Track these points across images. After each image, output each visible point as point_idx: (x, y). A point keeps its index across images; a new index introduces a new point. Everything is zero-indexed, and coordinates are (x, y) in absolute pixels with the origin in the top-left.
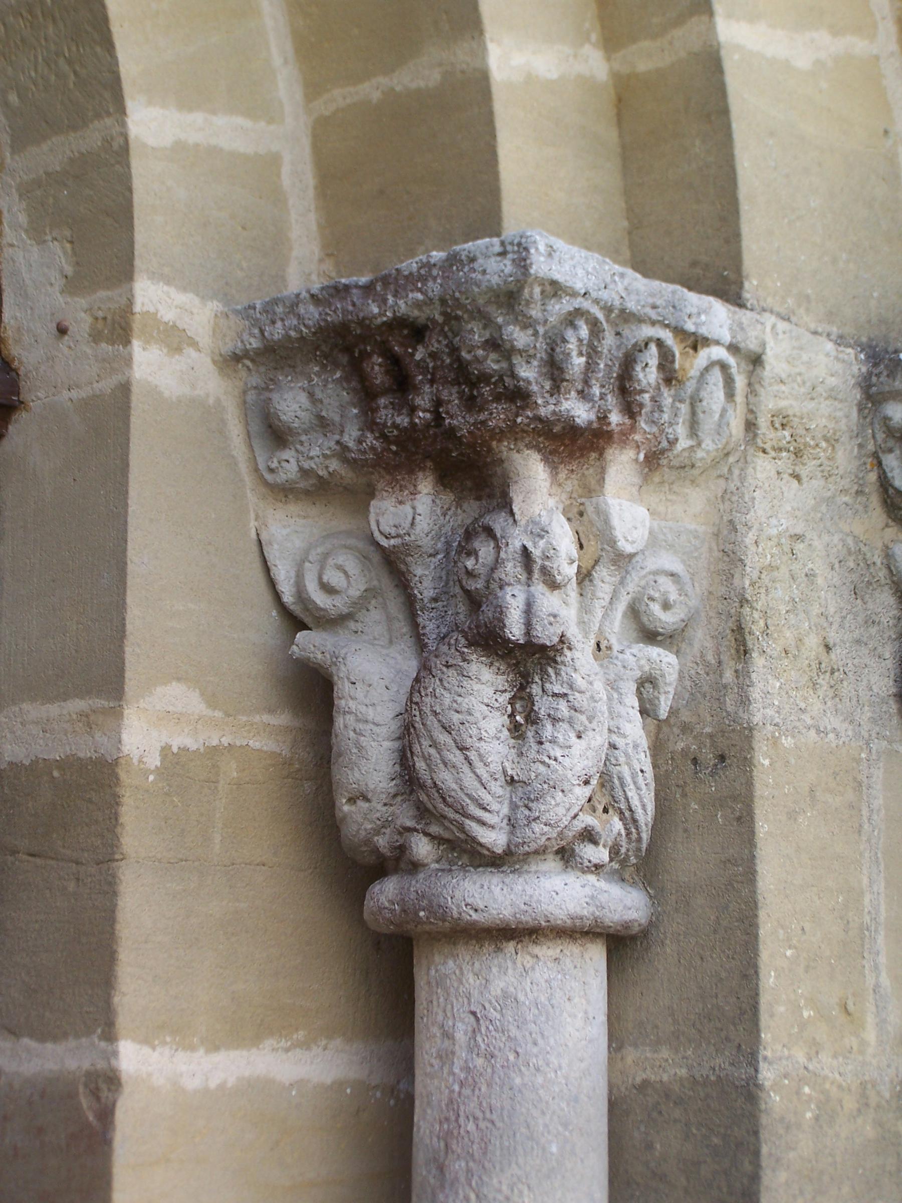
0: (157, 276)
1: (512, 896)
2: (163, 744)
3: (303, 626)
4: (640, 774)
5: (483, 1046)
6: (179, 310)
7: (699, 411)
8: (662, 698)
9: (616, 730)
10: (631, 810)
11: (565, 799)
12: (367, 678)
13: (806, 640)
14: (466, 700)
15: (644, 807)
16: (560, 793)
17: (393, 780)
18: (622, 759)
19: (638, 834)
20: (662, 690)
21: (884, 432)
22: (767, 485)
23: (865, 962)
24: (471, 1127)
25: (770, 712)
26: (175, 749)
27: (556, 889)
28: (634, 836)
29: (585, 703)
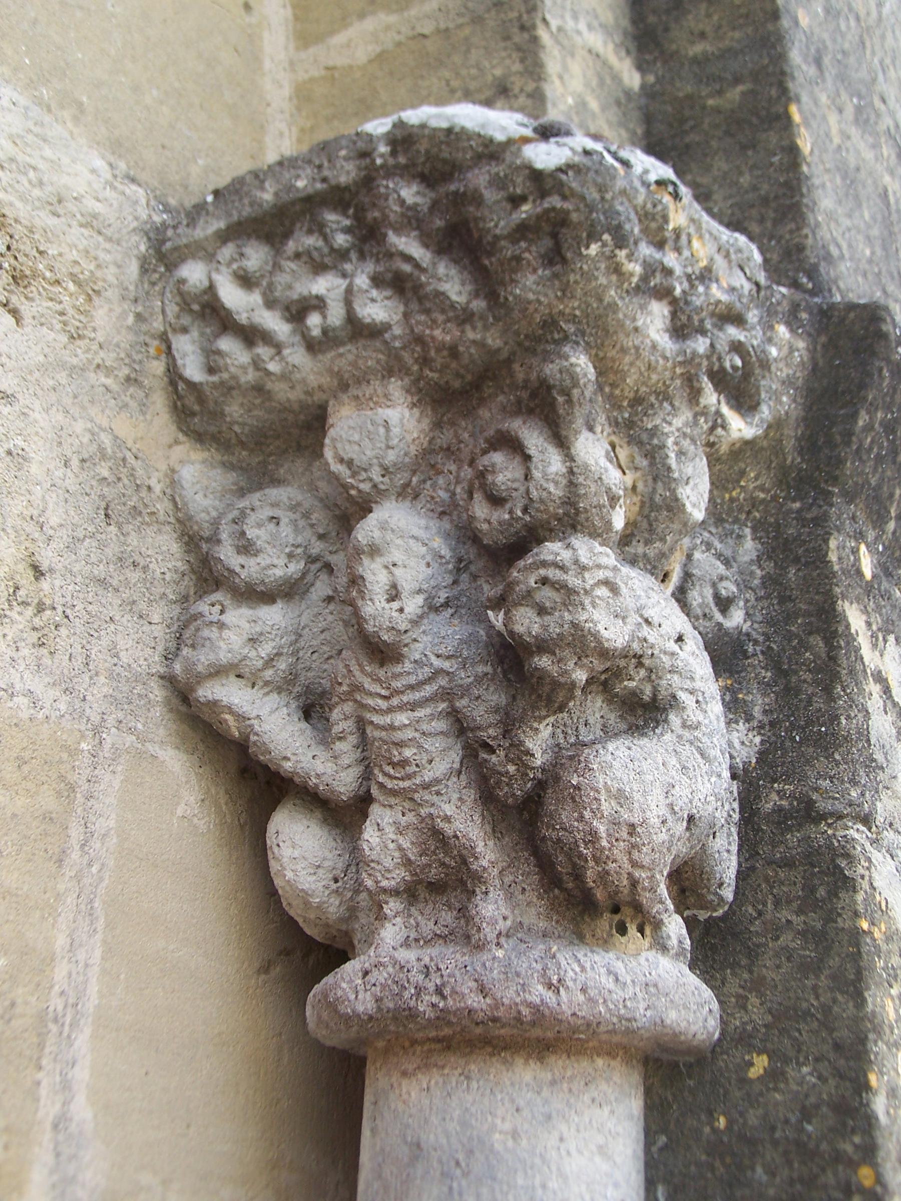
21: (177, 304)
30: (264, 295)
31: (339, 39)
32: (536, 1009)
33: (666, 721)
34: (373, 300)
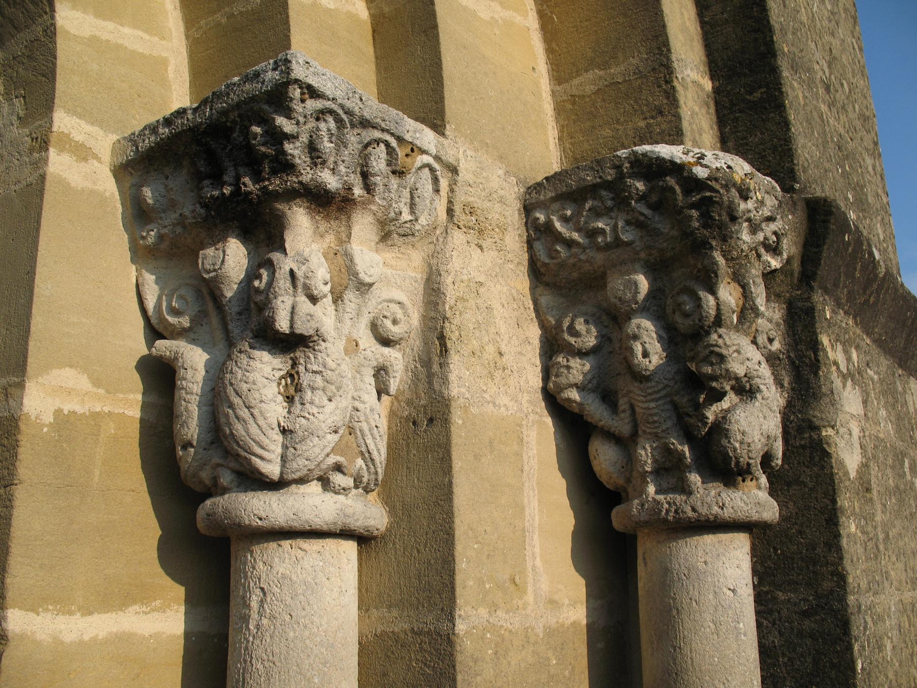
1: (285, 509)
2: (56, 408)
3: (162, 337)
4: (375, 429)
5: (268, 611)
6: (87, 136)
8: (392, 381)
10: (369, 452)
13: (486, 348)
14: (252, 375)
15: (378, 450)
16: (317, 438)
18: (362, 418)
19: (375, 468)
20: (391, 375)
22: (460, 248)
24: (260, 666)
25: (463, 390)
26: (66, 412)
28: (372, 470)
29: (335, 378)
30: (574, 225)
31: (576, 82)
32: (716, 517)
33: (756, 397)
34: (627, 231)
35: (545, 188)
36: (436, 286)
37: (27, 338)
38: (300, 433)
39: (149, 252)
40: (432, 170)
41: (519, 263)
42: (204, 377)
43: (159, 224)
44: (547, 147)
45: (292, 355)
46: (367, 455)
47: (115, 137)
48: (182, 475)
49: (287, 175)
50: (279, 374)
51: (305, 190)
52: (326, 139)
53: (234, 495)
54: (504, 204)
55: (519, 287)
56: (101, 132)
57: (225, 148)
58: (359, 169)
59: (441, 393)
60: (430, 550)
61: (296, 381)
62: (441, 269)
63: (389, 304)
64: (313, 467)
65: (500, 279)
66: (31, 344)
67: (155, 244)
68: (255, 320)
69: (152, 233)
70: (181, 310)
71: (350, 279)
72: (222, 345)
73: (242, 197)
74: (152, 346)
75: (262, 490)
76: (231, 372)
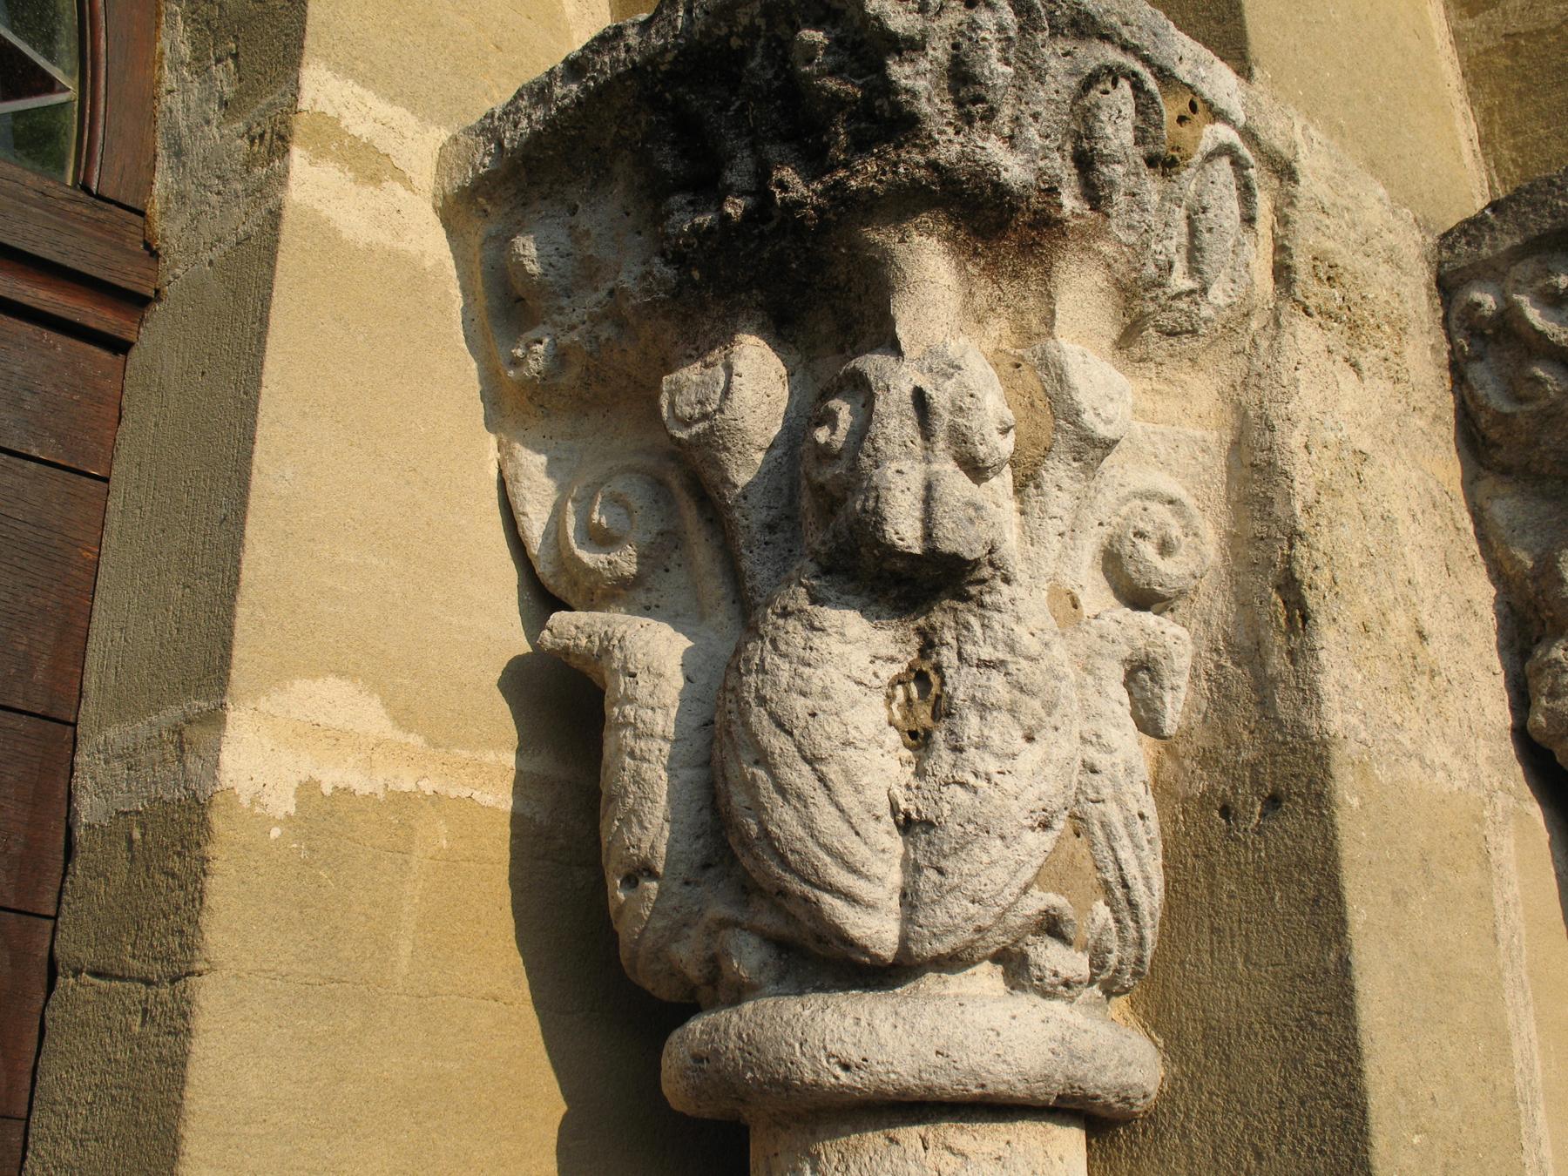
0: (345, 69)
1: (913, 1040)
2: (304, 779)
7: (1202, 227)
8: (1168, 697)
9: (1094, 739)
10: (1125, 885)
11: (1007, 853)
12: (655, 664)
13: (1391, 616)
14: (819, 672)
15: (1147, 879)
16: (999, 842)
17: (698, 837)
18: (1107, 792)
19: (1139, 929)
20: (1167, 683)
22: (1314, 363)
23: (1524, 1158)
25: (1354, 720)
26: (327, 790)
27: (995, 1025)
28: (1132, 934)
29: (1039, 678)
35: (1492, 228)
36: (1264, 456)
37: (233, 597)
38: (953, 828)
39: (530, 399)
40: (1238, 164)
41: (1436, 418)
42: (682, 692)
43: (555, 325)
44: (1459, 158)
45: (921, 621)
46: (1119, 893)
47: (444, 135)
48: (624, 954)
49: (896, 148)
50: (890, 671)
51: (943, 184)
52: (994, 52)
53: (770, 1002)
54: (1399, 267)
55: (1441, 474)
56: (412, 121)
57: (725, 107)
58: (1068, 147)
59: (1299, 729)
60: (1294, 1151)
61: (935, 690)
62: (1272, 413)
63: (1147, 504)
64: (989, 922)
65: (1403, 452)
66: (242, 611)
67: (547, 375)
68: (816, 538)
69: (539, 348)
70: (614, 532)
71: (1057, 429)
72: (723, 615)
73: (773, 224)
74: (542, 625)
75: (845, 989)
76: (762, 669)
